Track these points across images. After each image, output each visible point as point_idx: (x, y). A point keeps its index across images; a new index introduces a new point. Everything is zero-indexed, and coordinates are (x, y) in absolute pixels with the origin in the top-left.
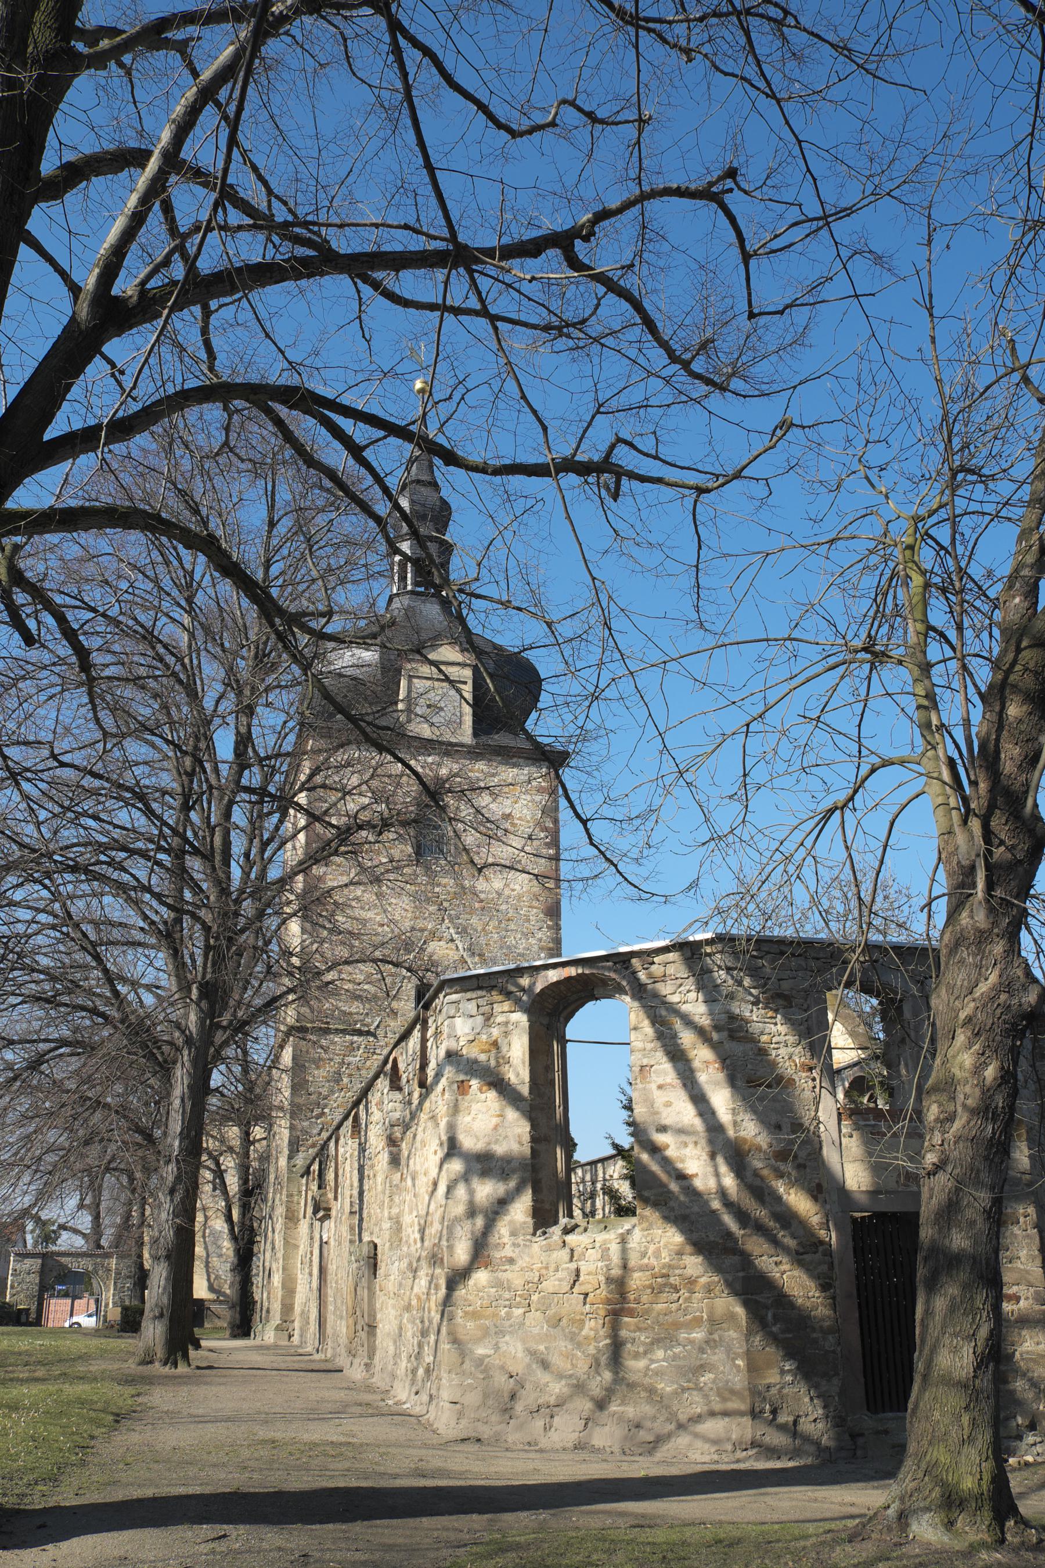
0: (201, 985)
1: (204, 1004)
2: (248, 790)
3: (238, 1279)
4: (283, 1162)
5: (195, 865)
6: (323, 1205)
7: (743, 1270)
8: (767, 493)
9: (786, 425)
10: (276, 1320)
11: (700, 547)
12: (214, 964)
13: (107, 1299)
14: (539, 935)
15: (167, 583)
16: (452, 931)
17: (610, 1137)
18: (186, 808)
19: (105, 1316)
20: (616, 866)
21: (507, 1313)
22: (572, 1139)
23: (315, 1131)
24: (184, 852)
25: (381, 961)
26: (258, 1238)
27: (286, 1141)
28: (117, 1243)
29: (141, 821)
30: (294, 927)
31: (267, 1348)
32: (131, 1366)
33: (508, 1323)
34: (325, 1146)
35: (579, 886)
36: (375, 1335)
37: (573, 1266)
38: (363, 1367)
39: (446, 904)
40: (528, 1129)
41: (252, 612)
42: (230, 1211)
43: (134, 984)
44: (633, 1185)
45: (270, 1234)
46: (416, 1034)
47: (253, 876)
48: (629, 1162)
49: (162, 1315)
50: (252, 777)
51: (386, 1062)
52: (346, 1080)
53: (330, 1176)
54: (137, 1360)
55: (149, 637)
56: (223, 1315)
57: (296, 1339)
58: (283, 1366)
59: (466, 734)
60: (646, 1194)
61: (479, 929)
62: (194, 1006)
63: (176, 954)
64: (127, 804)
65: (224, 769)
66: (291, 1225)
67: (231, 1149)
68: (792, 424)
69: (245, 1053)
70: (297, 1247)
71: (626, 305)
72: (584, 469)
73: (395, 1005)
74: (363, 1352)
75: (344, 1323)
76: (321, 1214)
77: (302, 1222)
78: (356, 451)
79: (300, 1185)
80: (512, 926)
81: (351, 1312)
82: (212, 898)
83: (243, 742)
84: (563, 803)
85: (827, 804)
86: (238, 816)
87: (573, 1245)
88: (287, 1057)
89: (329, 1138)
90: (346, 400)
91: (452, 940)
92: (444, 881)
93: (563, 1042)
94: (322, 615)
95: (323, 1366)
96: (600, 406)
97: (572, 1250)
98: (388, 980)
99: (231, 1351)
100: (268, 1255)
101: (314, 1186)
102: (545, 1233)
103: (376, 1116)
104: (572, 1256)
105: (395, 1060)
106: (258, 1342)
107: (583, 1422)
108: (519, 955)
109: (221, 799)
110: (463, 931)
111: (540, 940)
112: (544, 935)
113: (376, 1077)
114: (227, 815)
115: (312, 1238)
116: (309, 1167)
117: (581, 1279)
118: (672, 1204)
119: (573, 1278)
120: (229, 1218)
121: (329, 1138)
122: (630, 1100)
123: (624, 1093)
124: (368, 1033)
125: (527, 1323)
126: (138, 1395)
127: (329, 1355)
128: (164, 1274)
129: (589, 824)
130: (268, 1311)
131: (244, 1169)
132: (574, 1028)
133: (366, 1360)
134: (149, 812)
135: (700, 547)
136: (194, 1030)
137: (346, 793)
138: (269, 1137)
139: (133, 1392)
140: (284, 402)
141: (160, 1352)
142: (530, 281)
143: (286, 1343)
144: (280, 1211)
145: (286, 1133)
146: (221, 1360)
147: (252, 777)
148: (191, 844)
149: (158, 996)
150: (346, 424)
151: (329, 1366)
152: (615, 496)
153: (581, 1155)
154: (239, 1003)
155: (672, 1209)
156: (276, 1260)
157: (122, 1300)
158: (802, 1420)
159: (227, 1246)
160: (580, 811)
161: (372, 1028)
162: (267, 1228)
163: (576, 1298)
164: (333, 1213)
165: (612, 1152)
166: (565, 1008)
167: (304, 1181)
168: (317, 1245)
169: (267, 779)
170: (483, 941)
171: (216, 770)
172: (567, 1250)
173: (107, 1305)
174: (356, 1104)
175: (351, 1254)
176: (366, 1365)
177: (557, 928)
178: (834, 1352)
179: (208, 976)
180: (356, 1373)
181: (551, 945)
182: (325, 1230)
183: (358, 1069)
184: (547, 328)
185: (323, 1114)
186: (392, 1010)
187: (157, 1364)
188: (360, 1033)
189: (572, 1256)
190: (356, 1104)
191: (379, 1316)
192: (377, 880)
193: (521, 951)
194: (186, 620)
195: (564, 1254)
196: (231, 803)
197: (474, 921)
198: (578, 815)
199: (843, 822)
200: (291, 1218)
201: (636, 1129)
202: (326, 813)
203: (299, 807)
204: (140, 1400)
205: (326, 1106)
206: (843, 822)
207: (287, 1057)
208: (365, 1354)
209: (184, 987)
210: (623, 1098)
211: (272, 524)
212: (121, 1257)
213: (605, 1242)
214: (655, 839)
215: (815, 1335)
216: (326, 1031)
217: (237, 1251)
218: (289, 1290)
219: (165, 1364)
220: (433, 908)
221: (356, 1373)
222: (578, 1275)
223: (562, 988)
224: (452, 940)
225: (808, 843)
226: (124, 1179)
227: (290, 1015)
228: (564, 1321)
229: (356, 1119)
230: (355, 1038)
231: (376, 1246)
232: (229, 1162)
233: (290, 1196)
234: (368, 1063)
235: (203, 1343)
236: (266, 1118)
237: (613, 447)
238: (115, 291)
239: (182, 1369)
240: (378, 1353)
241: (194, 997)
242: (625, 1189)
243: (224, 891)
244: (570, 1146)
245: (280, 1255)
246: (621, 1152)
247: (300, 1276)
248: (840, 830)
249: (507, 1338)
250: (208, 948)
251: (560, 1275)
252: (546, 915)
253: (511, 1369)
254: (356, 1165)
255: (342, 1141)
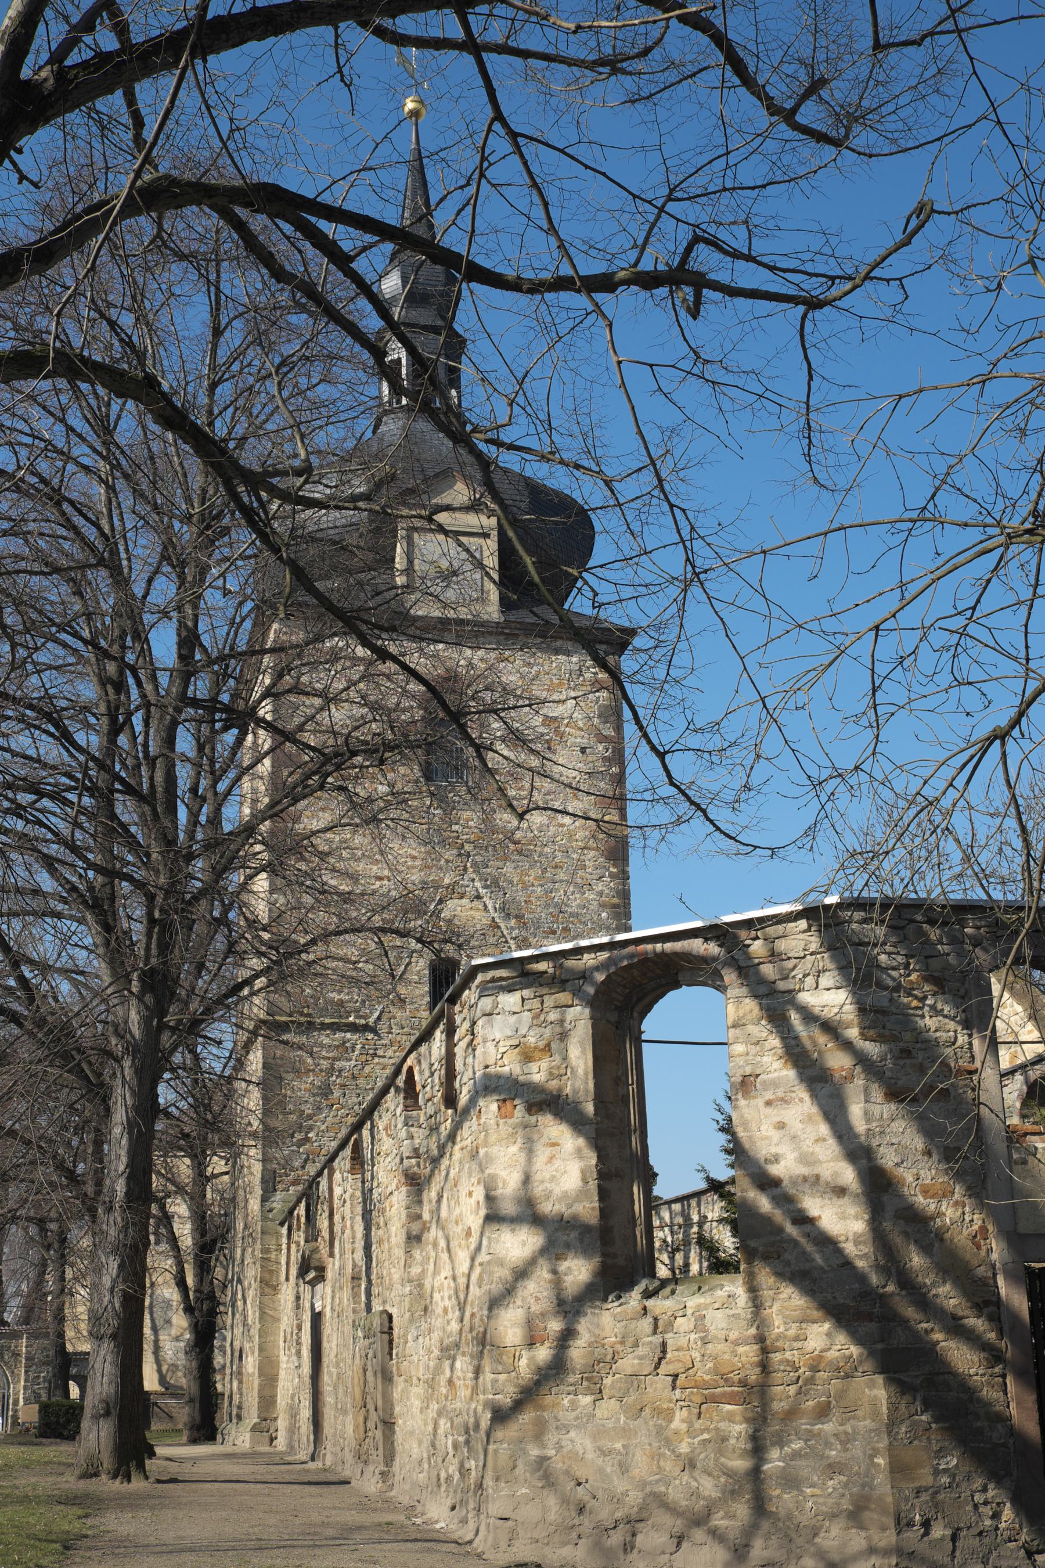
0: (143, 972)
1: (149, 999)
2: (195, 703)
3: (194, 1364)
4: (254, 1205)
5: (126, 810)
6: (314, 1263)
7: (882, 1341)
8: (902, 298)
9: (924, 212)
10: (252, 1417)
11: (811, 378)
12: (159, 946)
13: (16, 1394)
14: (600, 887)
15: (76, 420)
16: (478, 884)
17: (703, 1170)
18: (115, 730)
19: (15, 1417)
20: (704, 811)
21: (572, 1402)
22: (651, 1168)
23: (297, 1164)
24: (113, 791)
25: (383, 930)
26: (222, 1308)
27: (258, 1176)
28: (28, 1316)
29: (51, 750)
30: (262, 883)
31: (244, 1455)
32: (70, 1482)
33: (572, 1415)
34: (313, 1183)
35: (656, 834)
36: (393, 1432)
37: (657, 1339)
38: (378, 1476)
39: (468, 847)
40: (594, 1162)
41: (194, 465)
42: (181, 1272)
43: (44, 968)
44: (735, 1231)
45: (240, 1303)
46: (439, 1035)
47: (203, 819)
48: (730, 1202)
49: (107, 1414)
50: (201, 687)
51: (397, 1072)
52: (337, 1093)
53: (323, 1223)
54: (77, 1472)
55: (57, 498)
56: (183, 1413)
57: (281, 1443)
58: (269, 1478)
59: (492, 611)
60: (753, 1244)
61: (515, 880)
62: (134, 1002)
63: (108, 927)
64: (30, 726)
65: (163, 679)
66: (267, 1290)
67: (180, 1190)
68: (933, 211)
69: (196, 1057)
70: (278, 1320)
71: (704, 39)
72: (649, 281)
73: (402, 990)
74: (377, 1457)
75: (350, 1418)
76: (312, 1275)
77: (284, 1287)
78: (341, 260)
79: (278, 1235)
80: (562, 876)
81: (360, 1403)
82: (155, 856)
83: (189, 641)
84: (625, 706)
85: (983, 731)
86: (185, 743)
87: (657, 1312)
88: (255, 1060)
89: (320, 1174)
90: (326, 198)
91: (479, 897)
92: (466, 815)
93: (638, 1041)
94: (298, 473)
95: (322, 1478)
96: (672, 191)
97: (656, 1319)
98: (392, 955)
99: (195, 1460)
100: (238, 1331)
101: (300, 1237)
102: (619, 1297)
103: (386, 1144)
104: (656, 1327)
105: (410, 1070)
106: (227, 1448)
107: (675, 1541)
108: (572, 915)
109: (162, 718)
110: (494, 884)
111: (601, 894)
112: (605, 886)
113: (384, 1091)
114: (170, 741)
115: (298, 1307)
116: (291, 1212)
117: (668, 1356)
118: (787, 1256)
119: (658, 1353)
120: (181, 1283)
121: (320, 1174)
122: (730, 1120)
123: (720, 1110)
124: (366, 1028)
125: (599, 1415)
126: (86, 1516)
127: (328, 1463)
128: (109, 1359)
129: (668, 757)
130: (240, 1407)
131: (200, 1218)
132: (652, 1025)
133: (382, 1467)
134: (65, 737)
135: (811, 378)
136: (137, 1033)
137: (329, 699)
138: (235, 1171)
139: (80, 1512)
140: (247, 205)
141: (107, 1461)
142: (575, 32)
143: (266, 1449)
144: (251, 1274)
145: (257, 1168)
146: (186, 1471)
147: (201, 687)
148: (122, 781)
149: (75, 984)
150: (327, 227)
151: (332, 1478)
152: (695, 313)
153: (662, 1189)
154: (192, 991)
155: (788, 1263)
156: (251, 1339)
157: (38, 1396)
158: (964, 1533)
159: (180, 1322)
160: (655, 741)
161: (371, 1020)
162: (234, 1294)
163: (662, 1382)
164: (329, 1274)
165: (703, 1185)
166: (639, 1000)
167: (284, 1231)
168: (307, 1317)
169: (217, 687)
170: (521, 897)
171: (154, 678)
172: (649, 1320)
173: (16, 1402)
174: (357, 1127)
175: (355, 1326)
176: (382, 1473)
177: (624, 876)
178: (1004, 1445)
179: (154, 961)
180: (370, 1484)
181: (616, 900)
182: (318, 1296)
183: (354, 1078)
184: (592, 65)
185: (307, 1140)
186: (398, 996)
187: (104, 1477)
188: (354, 1028)
189: (656, 1327)
190: (357, 1127)
191: (397, 1410)
192: (374, 820)
193: (574, 909)
194: (103, 467)
195: (646, 1324)
196: (174, 724)
197: (508, 869)
198: (653, 748)
199: (1004, 754)
200: (268, 1285)
201: (737, 1151)
202: (301, 728)
203: (261, 722)
204: (90, 1522)
205: (310, 1129)
206: (1004, 754)
207: (255, 1060)
208: (381, 1458)
209: (121, 977)
210: (720, 1117)
211: (217, 332)
212: (33, 1336)
213: (699, 1308)
214: (755, 781)
215: (979, 1424)
216: (310, 1027)
217: (195, 1327)
218: (269, 1376)
219: (115, 1477)
220: (450, 854)
221: (370, 1484)
222: (664, 1351)
223: (636, 973)
224: (479, 897)
225: (960, 782)
226: (33, 1230)
227: (257, 1007)
228: (647, 1411)
229: (357, 1149)
230: (348, 1035)
231: (390, 1317)
232: (179, 1208)
233: (266, 1250)
234: (367, 1069)
235: (159, 1450)
236: (231, 1147)
237: (689, 249)
238: (26, 73)
239: (137, 1484)
240: (397, 1459)
241: (134, 990)
242: (727, 1241)
243: (168, 840)
244: (649, 1177)
245: (255, 1332)
246: (715, 1187)
247: (283, 1358)
248: (1001, 766)
249: (572, 1434)
250: (152, 921)
251: (641, 1351)
252: (608, 859)
253: (578, 1474)
254: (359, 1209)
255: (337, 1176)
